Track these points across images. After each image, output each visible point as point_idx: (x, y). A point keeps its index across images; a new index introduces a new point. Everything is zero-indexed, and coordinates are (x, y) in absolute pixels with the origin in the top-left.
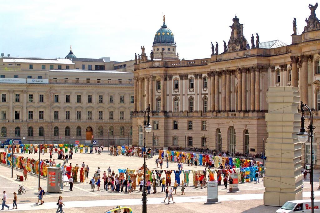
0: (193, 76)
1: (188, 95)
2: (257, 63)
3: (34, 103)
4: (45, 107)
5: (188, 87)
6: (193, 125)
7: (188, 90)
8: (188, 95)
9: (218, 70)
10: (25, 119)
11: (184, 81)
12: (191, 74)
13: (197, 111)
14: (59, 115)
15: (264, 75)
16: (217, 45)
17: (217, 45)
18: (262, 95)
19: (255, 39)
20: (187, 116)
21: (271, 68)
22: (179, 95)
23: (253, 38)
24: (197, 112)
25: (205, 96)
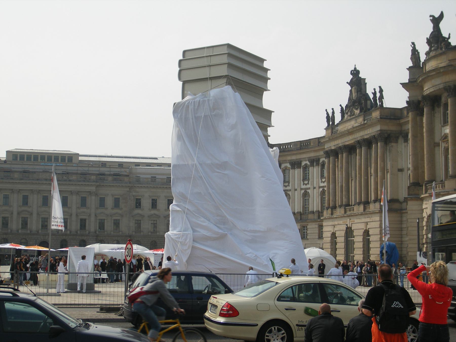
0: (308, 163)
1: (301, 189)
2: (379, 129)
3: (107, 208)
4: (122, 216)
5: (302, 179)
6: (308, 232)
7: (302, 183)
8: (301, 189)
9: (333, 148)
10: (92, 230)
11: (297, 171)
12: (306, 161)
13: (313, 211)
14: (142, 225)
15: (392, 146)
16: (333, 113)
17: (333, 113)
18: (390, 177)
19: (378, 95)
20: (301, 219)
21: (403, 136)
22: (290, 190)
23: (375, 94)
24: (313, 212)
25: (323, 189)
